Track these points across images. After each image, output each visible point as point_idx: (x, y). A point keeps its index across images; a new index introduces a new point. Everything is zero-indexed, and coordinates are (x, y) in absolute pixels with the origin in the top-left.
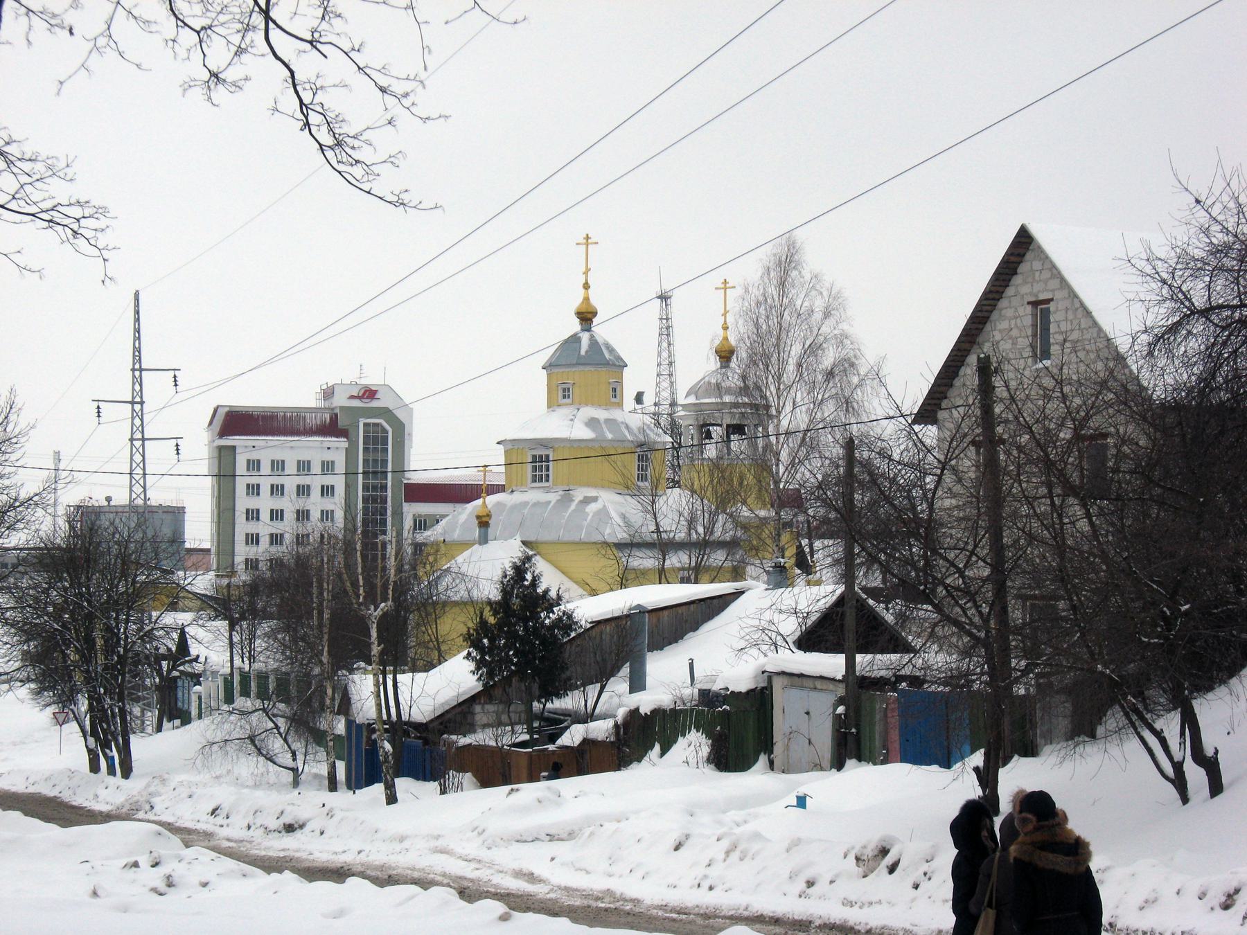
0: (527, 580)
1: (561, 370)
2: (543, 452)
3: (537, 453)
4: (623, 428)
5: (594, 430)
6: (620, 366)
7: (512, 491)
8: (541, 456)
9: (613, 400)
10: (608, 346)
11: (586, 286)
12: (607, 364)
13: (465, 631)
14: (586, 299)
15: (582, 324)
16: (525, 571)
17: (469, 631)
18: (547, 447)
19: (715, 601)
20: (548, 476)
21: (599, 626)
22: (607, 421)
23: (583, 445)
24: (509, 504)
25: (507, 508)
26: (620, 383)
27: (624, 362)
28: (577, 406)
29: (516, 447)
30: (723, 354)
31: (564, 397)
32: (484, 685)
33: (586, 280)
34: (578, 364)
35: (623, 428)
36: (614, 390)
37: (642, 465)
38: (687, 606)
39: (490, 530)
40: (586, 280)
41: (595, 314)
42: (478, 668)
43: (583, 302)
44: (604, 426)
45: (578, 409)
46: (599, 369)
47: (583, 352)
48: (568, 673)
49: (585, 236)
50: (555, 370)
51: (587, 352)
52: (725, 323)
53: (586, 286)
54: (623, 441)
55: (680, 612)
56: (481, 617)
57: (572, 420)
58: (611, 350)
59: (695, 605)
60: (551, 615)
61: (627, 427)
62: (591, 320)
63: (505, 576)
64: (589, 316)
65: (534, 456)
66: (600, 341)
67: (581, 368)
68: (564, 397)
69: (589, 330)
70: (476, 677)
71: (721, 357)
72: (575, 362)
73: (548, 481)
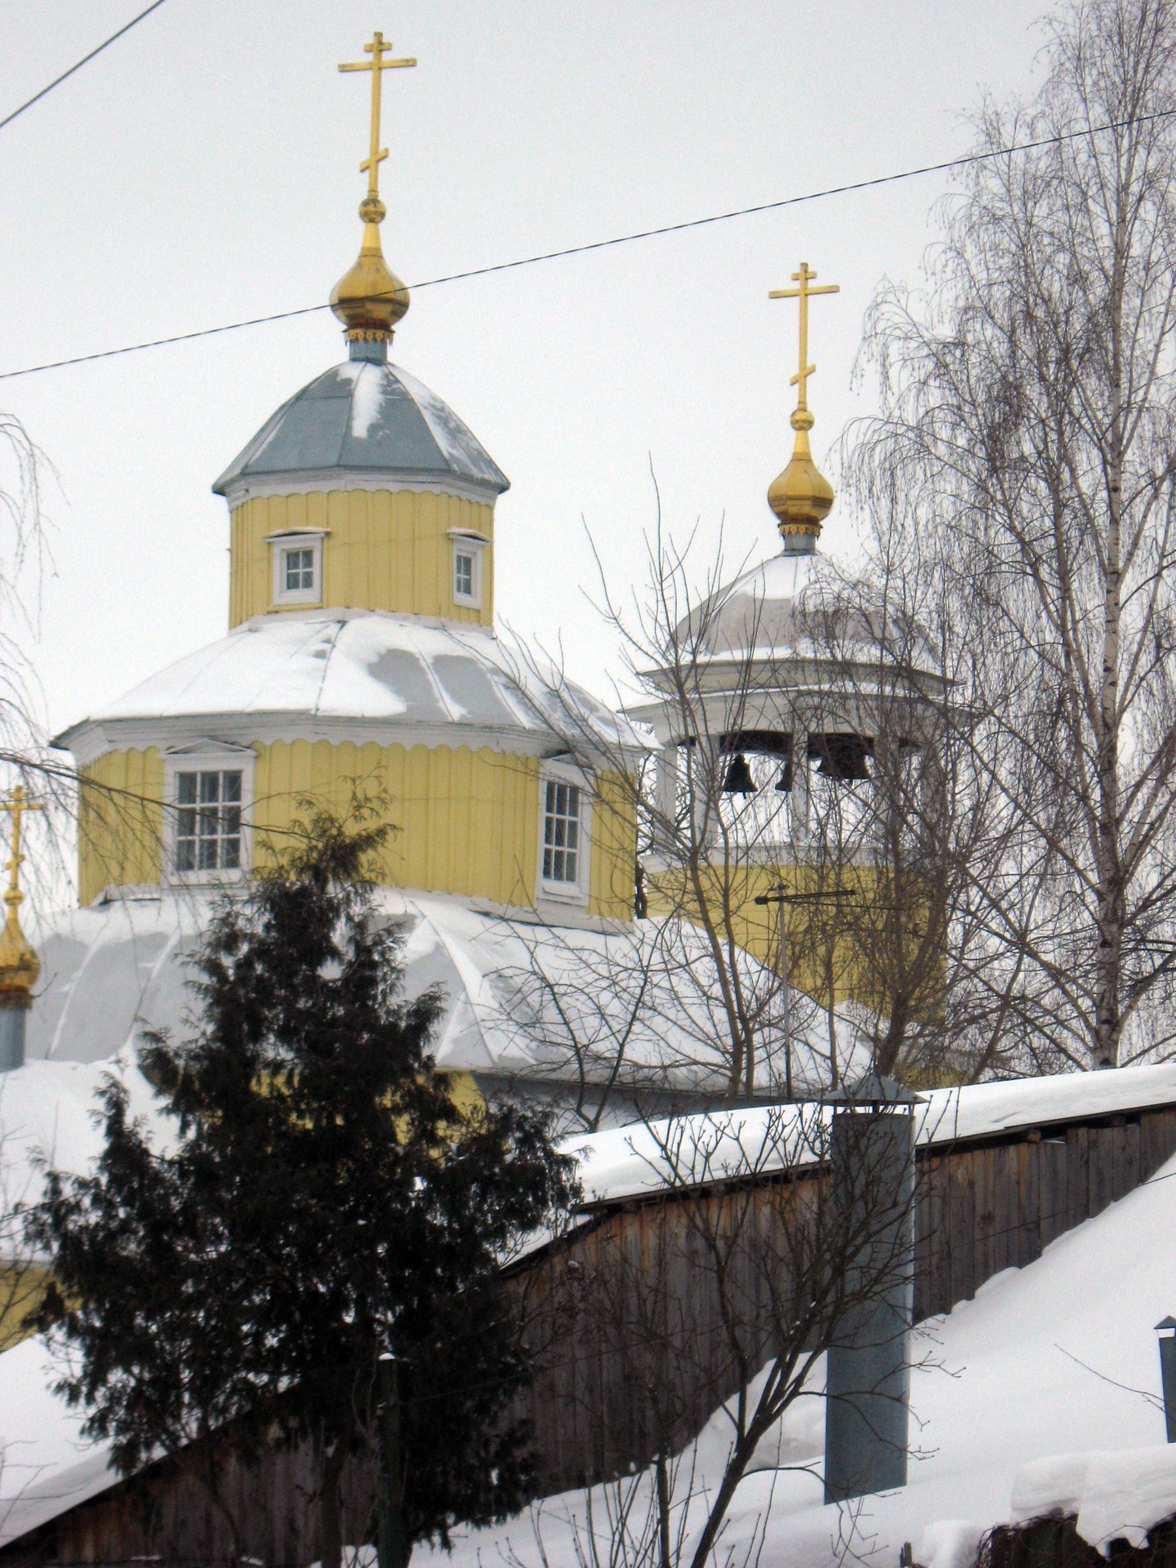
0: (334, 953)
1: (284, 490)
2: (219, 762)
3: (198, 764)
4: (497, 683)
5: (399, 690)
6: (484, 483)
7: (106, 902)
8: (211, 780)
9: (462, 598)
10: (444, 416)
11: (372, 212)
12: (444, 470)
13: (34, 1194)
14: (372, 256)
15: (353, 341)
16: (328, 913)
17: (55, 1191)
18: (232, 745)
19: (1108, 1134)
20: (234, 845)
21: (614, 1226)
22: (442, 662)
23: (362, 737)
24: (95, 944)
25: (92, 952)
26: (481, 539)
27: (497, 471)
28: (337, 612)
29: (123, 747)
30: (793, 510)
31: (292, 582)
32: (123, 1457)
33: (373, 190)
34: (343, 467)
35: (497, 683)
36: (465, 564)
37: (559, 842)
38: (992, 1153)
39: (32, 1018)
40: (373, 190)
41: (400, 307)
42: (95, 1375)
43: (359, 266)
44: (433, 678)
45: (343, 623)
46: (417, 488)
47: (359, 429)
48: (519, 1407)
49: (371, 40)
50: (265, 490)
51: (373, 429)
52: (802, 407)
53: (372, 212)
54: (502, 729)
55: (960, 1175)
56: (116, 1128)
57: (321, 655)
58: (457, 431)
59: (1024, 1147)
60: (442, 1128)
61: (514, 685)
62: (384, 327)
63: (229, 941)
64: (380, 311)
65: (187, 780)
66: (415, 392)
67: (352, 481)
68: (292, 582)
69: (379, 361)
70: (84, 1412)
71: (785, 518)
72: (333, 460)
73: (233, 863)
